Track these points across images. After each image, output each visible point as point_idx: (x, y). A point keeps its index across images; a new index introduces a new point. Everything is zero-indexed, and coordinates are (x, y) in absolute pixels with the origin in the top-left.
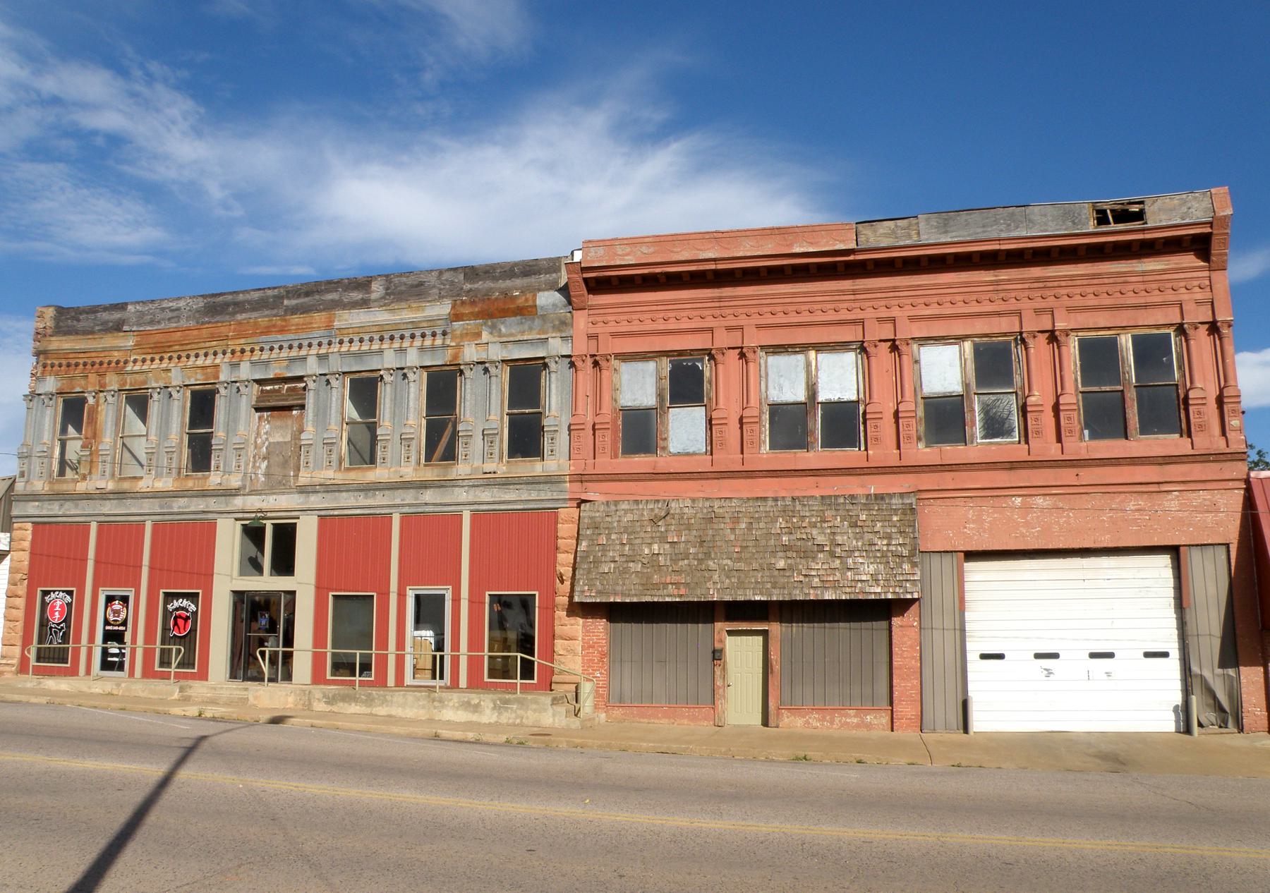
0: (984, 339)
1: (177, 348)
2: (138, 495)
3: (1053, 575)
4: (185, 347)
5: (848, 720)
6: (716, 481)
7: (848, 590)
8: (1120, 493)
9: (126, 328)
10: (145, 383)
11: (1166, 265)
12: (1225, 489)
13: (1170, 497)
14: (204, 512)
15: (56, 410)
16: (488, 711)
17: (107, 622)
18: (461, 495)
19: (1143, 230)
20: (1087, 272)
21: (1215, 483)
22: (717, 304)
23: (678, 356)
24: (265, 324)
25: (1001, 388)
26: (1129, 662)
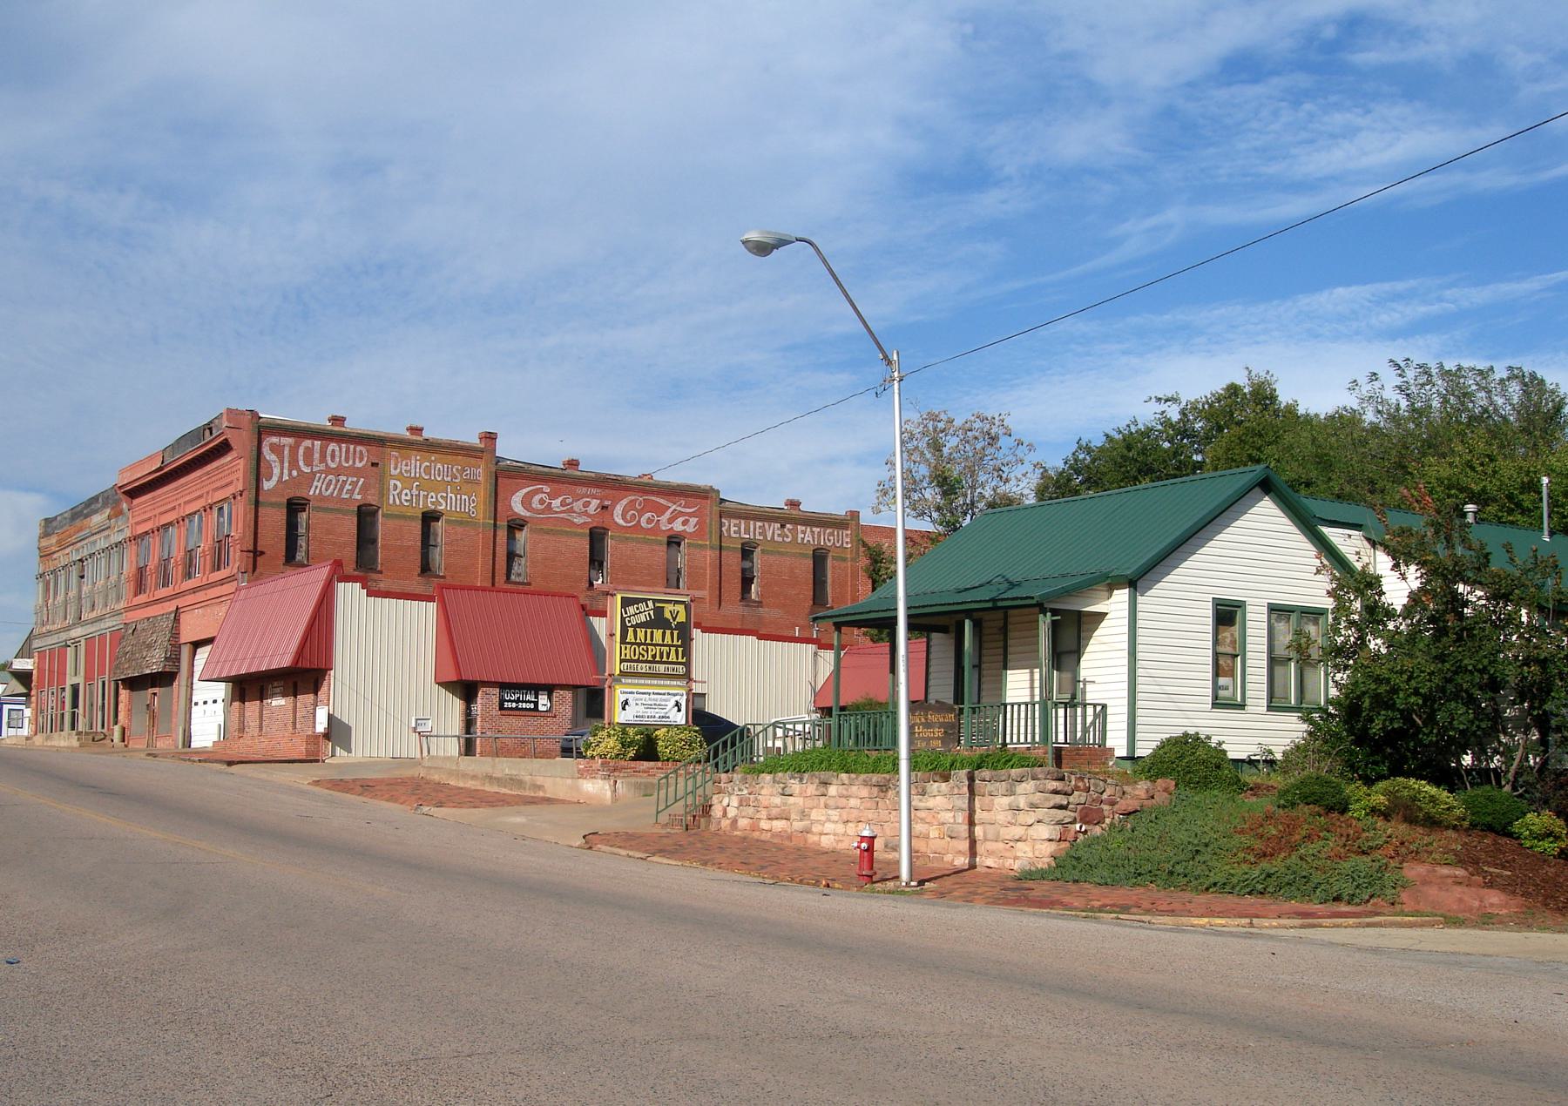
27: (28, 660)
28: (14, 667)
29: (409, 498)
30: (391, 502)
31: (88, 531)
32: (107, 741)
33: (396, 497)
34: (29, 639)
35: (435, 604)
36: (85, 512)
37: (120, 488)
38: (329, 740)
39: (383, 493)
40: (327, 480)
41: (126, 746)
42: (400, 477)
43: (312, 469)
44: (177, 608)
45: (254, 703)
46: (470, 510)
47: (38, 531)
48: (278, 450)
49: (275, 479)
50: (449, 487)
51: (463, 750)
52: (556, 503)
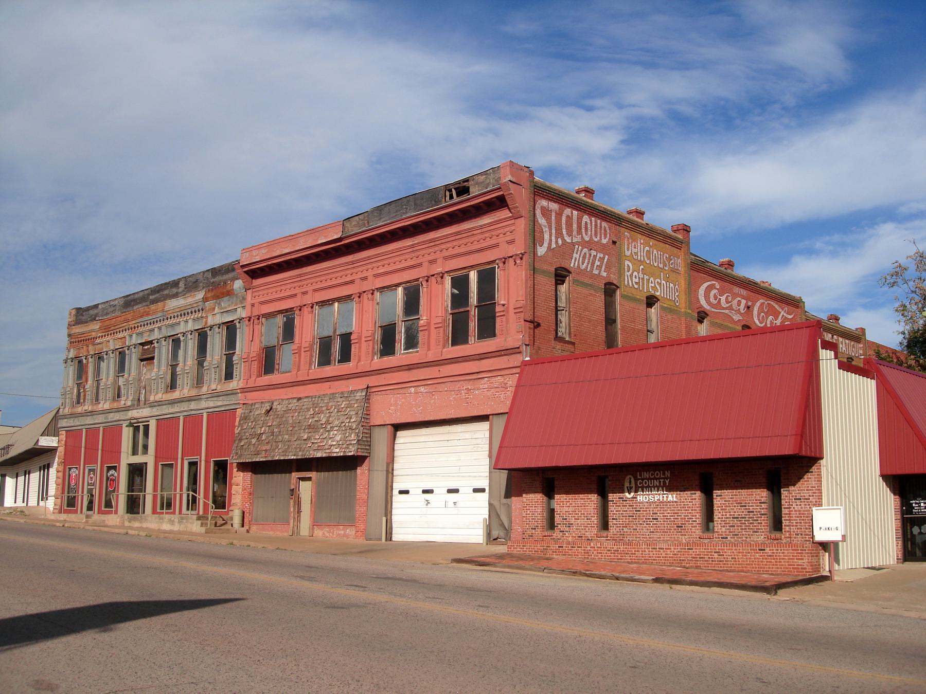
0: (408, 284)
1: (113, 328)
2: (97, 413)
3: (435, 438)
4: (117, 327)
5: (340, 532)
6: (292, 388)
7: (327, 451)
8: (459, 381)
9: (97, 318)
10: (103, 349)
11: (493, 219)
14: (119, 420)
15: (75, 367)
16: (176, 524)
17: (88, 485)
18: (204, 404)
19: (469, 199)
22: (299, 279)
23: (286, 312)
24: (142, 311)
25: (413, 316)
26: (415, 489)
27: (54, 438)
28: (40, 444)
29: (637, 280)
30: (626, 283)
31: (160, 314)
32: (228, 526)
33: (629, 277)
34: (56, 418)
35: (875, 381)
36: (151, 297)
37: (243, 266)
38: (825, 551)
39: (621, 274)
40: (583, 253)
41: (248, 531)
42: (631, 258)
43: (572, 240)
44: (368, 387)
45: (590, 496)
46: (675, 298)
47: (67, 319)
48: (546, 212)
49: (546, 245)
50: (662, 273)
51: (900, 556)
52: (723, 298)
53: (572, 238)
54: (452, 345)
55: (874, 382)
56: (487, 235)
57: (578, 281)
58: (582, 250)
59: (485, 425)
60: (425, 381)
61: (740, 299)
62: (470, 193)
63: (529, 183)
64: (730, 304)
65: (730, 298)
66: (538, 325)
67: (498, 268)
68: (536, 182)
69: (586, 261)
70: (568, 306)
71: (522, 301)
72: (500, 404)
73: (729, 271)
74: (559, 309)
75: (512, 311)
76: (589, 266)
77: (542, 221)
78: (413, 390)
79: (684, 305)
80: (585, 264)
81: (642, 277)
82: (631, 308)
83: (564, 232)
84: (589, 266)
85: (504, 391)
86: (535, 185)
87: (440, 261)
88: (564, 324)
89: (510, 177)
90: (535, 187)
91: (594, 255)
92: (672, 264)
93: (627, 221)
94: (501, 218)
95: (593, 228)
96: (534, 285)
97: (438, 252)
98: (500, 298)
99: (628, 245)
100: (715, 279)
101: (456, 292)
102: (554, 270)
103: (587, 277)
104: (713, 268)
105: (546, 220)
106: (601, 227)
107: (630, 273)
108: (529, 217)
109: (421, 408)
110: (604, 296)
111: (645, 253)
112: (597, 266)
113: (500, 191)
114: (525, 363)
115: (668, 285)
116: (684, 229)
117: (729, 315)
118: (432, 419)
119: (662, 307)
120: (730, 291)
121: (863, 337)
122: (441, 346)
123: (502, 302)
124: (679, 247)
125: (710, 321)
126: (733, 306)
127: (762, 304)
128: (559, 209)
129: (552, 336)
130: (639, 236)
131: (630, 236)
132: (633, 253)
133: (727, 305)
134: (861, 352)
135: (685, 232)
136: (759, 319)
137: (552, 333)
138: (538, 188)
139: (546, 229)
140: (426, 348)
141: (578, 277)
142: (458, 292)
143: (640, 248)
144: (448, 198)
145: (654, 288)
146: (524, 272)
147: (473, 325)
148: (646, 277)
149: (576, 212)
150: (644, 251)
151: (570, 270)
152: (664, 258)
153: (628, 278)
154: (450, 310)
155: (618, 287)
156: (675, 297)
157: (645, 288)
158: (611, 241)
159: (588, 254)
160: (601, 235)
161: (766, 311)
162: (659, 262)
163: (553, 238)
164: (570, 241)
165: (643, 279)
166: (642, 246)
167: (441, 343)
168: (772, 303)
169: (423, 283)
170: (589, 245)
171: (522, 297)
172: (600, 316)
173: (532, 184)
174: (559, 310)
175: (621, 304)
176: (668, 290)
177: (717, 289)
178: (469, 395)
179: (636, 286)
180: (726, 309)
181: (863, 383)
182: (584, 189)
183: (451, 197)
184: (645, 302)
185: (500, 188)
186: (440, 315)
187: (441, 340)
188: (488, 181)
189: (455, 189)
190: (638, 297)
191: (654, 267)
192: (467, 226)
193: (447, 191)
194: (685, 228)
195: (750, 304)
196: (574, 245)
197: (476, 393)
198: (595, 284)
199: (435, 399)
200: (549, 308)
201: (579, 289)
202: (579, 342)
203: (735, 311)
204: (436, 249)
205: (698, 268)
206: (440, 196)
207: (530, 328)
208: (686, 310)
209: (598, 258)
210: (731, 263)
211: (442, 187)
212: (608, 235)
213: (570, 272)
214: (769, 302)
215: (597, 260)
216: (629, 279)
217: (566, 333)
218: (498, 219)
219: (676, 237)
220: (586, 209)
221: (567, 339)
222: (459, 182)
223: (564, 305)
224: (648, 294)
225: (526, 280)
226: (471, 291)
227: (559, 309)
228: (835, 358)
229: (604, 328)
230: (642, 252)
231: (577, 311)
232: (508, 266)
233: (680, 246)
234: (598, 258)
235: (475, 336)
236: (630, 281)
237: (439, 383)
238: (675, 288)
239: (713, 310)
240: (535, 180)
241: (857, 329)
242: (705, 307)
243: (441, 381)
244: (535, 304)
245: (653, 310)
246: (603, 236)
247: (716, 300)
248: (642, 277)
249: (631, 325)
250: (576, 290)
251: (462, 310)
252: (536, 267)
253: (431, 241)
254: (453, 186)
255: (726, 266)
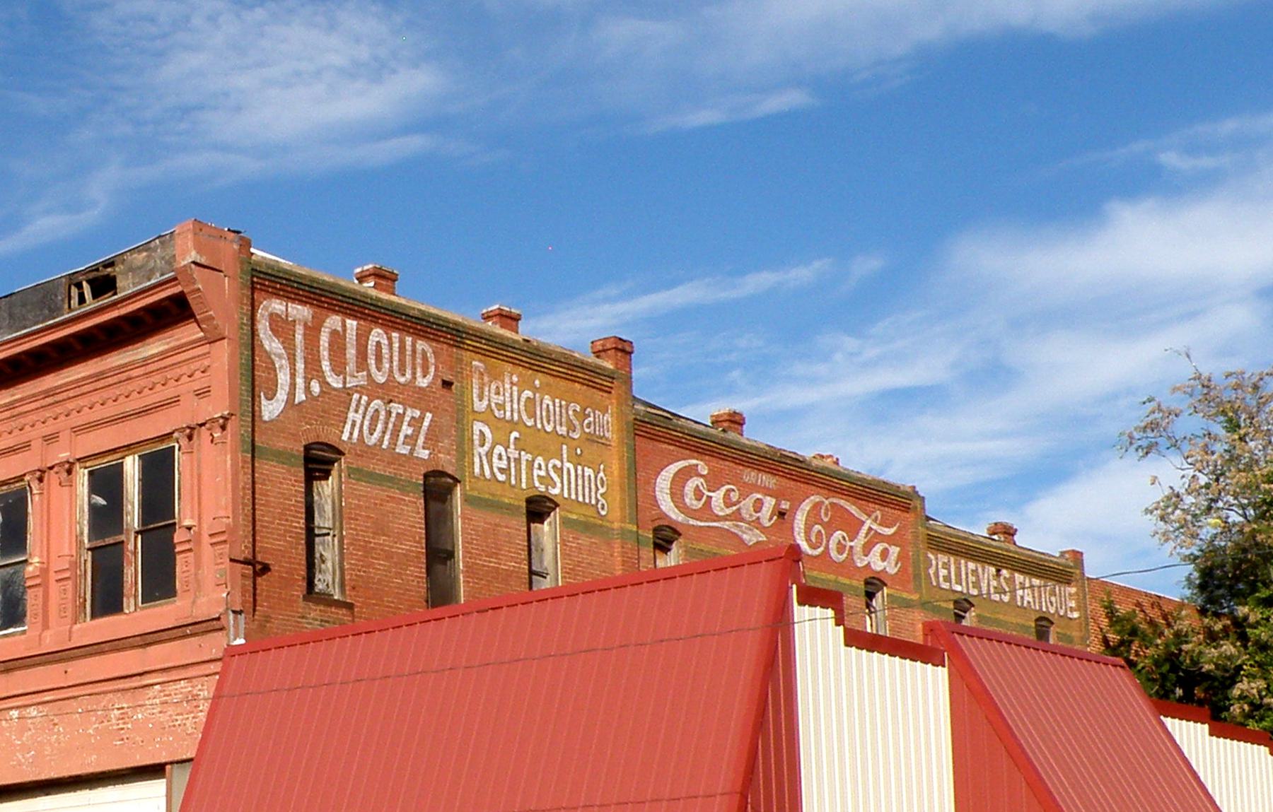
8: (105, 693)
11: (168, 343)
12: (207, 676)
13: (151, 694)
19: (114, 305)
20: (88, 373)
21: (196, 668)
29: (504, 464)
30: (477, 470)
33: (484, 458)
35: (946, 670)
39: (463, 450)
40: (371, 410)
42: (488, 417)
43: (345, 383)
46: (598, 501)
48: (281, 327)
49: (282, 395)
50: (565, 447)
52: (718, 497)
53: (345, 378)
54: (93, 616)
55: (942, 673)
56: (157, 378)
57: (358, 470)
58: (368, 404)
59: (155, 789)
60: (40, 695)
61: (759, 496)
62: (118, 290)
63: (239, 265)
64: (734, 508)
65: (735, 496)
66: (266, 569)
67: (179, 450)
68: (258, 263)
69: (380, 427)
70: (337, 524)
71: (224, 520)
72: (185, 740)
73: (732, 435)
74: (317, 531)
75: (206, 540)
76: (387, 437)
77: (271, 344)
78: (15, 713)
79: (618, 514)
80: (376, 435)
81: (517, 456)
82: (490, 524)
83: (326, 366)
84: (387, 437)
85: (192, 712)
86: (253, 269)
87: (65, 436)
88: (329, 564)
89: (194, 255)
90: (254, 273)
91: (398, 414)
92: (589, 426)
93: (476, 336)
94: (183, 341)
95: (396, 354)
96: (254, 483)
97: (62, 418)
98: (184, 514)
99: (481, 389)
100: (696, 454)
101: (101, 501)
102: (302, 449)
103: (384, 461)
104: (691, 429)
105: (283, 343)
106: (414, 351)
107: (486, 448)
108: (241, 339)
109: (33, 753)
110: (422, 501)
111: (522, 403)
112: (406, 436)
113: (176, 285)
114: (232, 652)
115: (580, 472)
116: (616, 349)
117: (732, 533)
118: (54, 775)
119: (566, 522)
120: (737, 480)
121: (1078, 572)
122: (69, 620)
123: (187, 523)
124: (607, 389)
125: (686, 546)
126: (743, 512)
127: (817, 506)
128: (313, 317)
129: (299, 589)
130: (509, 367)
131: (486, 369)
132: (493, 405)
133: (729, 511)
134: (1073, 604)
135: (620, 354)
136: (808, 540)
137: (299, 586)
138: (262, 276)
139: (282, 364)
140: (39, 625)
141: (359, 462)
142: (104, 503)
143: (511, 394)
144: (75, 301)
145: (547, 480)
146: (229, 457)
147: (133, 573)
148: (525, 457)
149: (355, 323)
150: (519, 400)
151: (340, 448)
152: (571, 413)
153: (481, 461)
154: (86, 541)
155: (457, 481)
156: (596, 498)
157: (524, 480)
158: (439, 382)
159: (383, 413)
160: (414, 369)
161: (826, 520)
162: (558, 422)
163: (300, 381)
164: (341, 386)
165: (518, 461)
166: (515, 388)
167: (69, 613)
168: (842, 502)
169: (32, 485)
170: (387, 392)
171: (226, 509)
172: (415, 545)
173: (247, 268)
174: (319, 535)
175: (464, 518)
176: (580, 482)
177: (702, 476)
178: (124, 723)
179: (501, 477)
180: (725, 518)
181: (870, 671)
182: (372, 271)
183: (82, 300)
184: (525, 511)
185: (175, 279)
186: (66, 552)
187: (70, 606)
188: (152, 264)
189: (89, 282)
190: (506, 501)
191: (546, 436)
192: (117, 360)
193: (73, 287)
194: (620, 347)
195: (785, 505)
196: (349, 394)
197: (138, 719)
198: (401, 475)
199: (59, 733)
200: (291, 532)
201: (363, 487)
202: (362, 602)
203: (749, 523)
204: (58, 410)
205: (652, 432)
206: (60, 298)
207: (243, 576)
208: (623, 525)
209: (407, 419)
210: (737, 418)
211: (64, 280)
212: (432, 369)
213: (341, 453)
214: (835, 500)
215: (405, 423)
216: (485, 462)
217: (334, 582)
218: (178, 343)
219: (600, 367)
220: (377, 315)
221: (336, 597)
222: (95, 269)
223: (329, 524)
224: (532, 493)
225: (235, 475)
226: (127, 498)
227: (317, 531)
228: (838, 624)
229: (424, 570)
230: (515, 401)
231: (357, 535)
232: (199, 445)
233: (609, 384)
234: (407, 419)
235: (136, 597)
236: (486, 467)
237: (68, 698)
238: (596, 477)
239: (692, 522)
240: (253, 257)
241: (1063, 554)
242: (674, 517)
243: (70, 695)
244: (258, 523)
245: (546, 526)
246: (419, 370)
247: (700, 500)
248: (517, 456)
249: (490, 562)
250: (355, 489)
251: (110, 540)
252: (258, 444)
253: (48, 393)
254: (84, 277)
255: (726, 424)
